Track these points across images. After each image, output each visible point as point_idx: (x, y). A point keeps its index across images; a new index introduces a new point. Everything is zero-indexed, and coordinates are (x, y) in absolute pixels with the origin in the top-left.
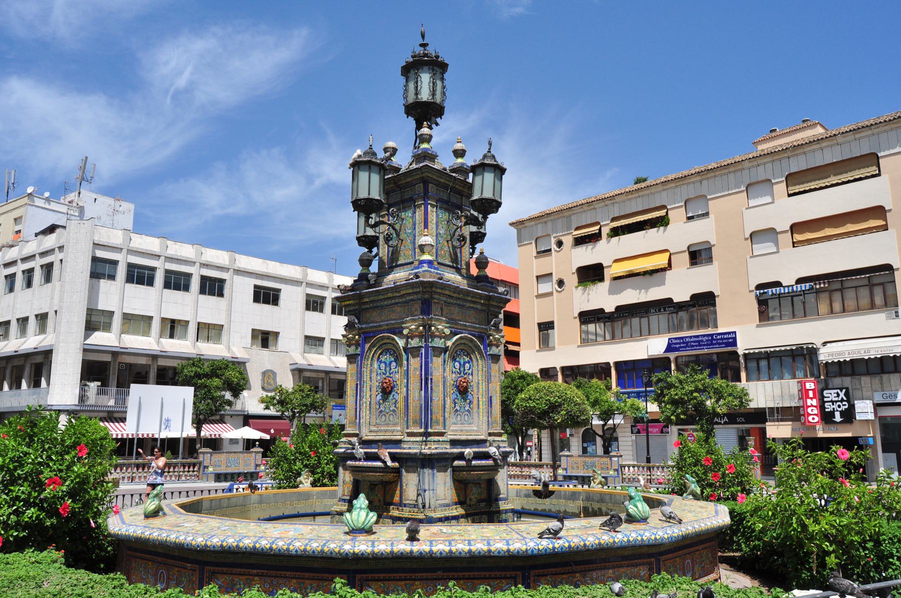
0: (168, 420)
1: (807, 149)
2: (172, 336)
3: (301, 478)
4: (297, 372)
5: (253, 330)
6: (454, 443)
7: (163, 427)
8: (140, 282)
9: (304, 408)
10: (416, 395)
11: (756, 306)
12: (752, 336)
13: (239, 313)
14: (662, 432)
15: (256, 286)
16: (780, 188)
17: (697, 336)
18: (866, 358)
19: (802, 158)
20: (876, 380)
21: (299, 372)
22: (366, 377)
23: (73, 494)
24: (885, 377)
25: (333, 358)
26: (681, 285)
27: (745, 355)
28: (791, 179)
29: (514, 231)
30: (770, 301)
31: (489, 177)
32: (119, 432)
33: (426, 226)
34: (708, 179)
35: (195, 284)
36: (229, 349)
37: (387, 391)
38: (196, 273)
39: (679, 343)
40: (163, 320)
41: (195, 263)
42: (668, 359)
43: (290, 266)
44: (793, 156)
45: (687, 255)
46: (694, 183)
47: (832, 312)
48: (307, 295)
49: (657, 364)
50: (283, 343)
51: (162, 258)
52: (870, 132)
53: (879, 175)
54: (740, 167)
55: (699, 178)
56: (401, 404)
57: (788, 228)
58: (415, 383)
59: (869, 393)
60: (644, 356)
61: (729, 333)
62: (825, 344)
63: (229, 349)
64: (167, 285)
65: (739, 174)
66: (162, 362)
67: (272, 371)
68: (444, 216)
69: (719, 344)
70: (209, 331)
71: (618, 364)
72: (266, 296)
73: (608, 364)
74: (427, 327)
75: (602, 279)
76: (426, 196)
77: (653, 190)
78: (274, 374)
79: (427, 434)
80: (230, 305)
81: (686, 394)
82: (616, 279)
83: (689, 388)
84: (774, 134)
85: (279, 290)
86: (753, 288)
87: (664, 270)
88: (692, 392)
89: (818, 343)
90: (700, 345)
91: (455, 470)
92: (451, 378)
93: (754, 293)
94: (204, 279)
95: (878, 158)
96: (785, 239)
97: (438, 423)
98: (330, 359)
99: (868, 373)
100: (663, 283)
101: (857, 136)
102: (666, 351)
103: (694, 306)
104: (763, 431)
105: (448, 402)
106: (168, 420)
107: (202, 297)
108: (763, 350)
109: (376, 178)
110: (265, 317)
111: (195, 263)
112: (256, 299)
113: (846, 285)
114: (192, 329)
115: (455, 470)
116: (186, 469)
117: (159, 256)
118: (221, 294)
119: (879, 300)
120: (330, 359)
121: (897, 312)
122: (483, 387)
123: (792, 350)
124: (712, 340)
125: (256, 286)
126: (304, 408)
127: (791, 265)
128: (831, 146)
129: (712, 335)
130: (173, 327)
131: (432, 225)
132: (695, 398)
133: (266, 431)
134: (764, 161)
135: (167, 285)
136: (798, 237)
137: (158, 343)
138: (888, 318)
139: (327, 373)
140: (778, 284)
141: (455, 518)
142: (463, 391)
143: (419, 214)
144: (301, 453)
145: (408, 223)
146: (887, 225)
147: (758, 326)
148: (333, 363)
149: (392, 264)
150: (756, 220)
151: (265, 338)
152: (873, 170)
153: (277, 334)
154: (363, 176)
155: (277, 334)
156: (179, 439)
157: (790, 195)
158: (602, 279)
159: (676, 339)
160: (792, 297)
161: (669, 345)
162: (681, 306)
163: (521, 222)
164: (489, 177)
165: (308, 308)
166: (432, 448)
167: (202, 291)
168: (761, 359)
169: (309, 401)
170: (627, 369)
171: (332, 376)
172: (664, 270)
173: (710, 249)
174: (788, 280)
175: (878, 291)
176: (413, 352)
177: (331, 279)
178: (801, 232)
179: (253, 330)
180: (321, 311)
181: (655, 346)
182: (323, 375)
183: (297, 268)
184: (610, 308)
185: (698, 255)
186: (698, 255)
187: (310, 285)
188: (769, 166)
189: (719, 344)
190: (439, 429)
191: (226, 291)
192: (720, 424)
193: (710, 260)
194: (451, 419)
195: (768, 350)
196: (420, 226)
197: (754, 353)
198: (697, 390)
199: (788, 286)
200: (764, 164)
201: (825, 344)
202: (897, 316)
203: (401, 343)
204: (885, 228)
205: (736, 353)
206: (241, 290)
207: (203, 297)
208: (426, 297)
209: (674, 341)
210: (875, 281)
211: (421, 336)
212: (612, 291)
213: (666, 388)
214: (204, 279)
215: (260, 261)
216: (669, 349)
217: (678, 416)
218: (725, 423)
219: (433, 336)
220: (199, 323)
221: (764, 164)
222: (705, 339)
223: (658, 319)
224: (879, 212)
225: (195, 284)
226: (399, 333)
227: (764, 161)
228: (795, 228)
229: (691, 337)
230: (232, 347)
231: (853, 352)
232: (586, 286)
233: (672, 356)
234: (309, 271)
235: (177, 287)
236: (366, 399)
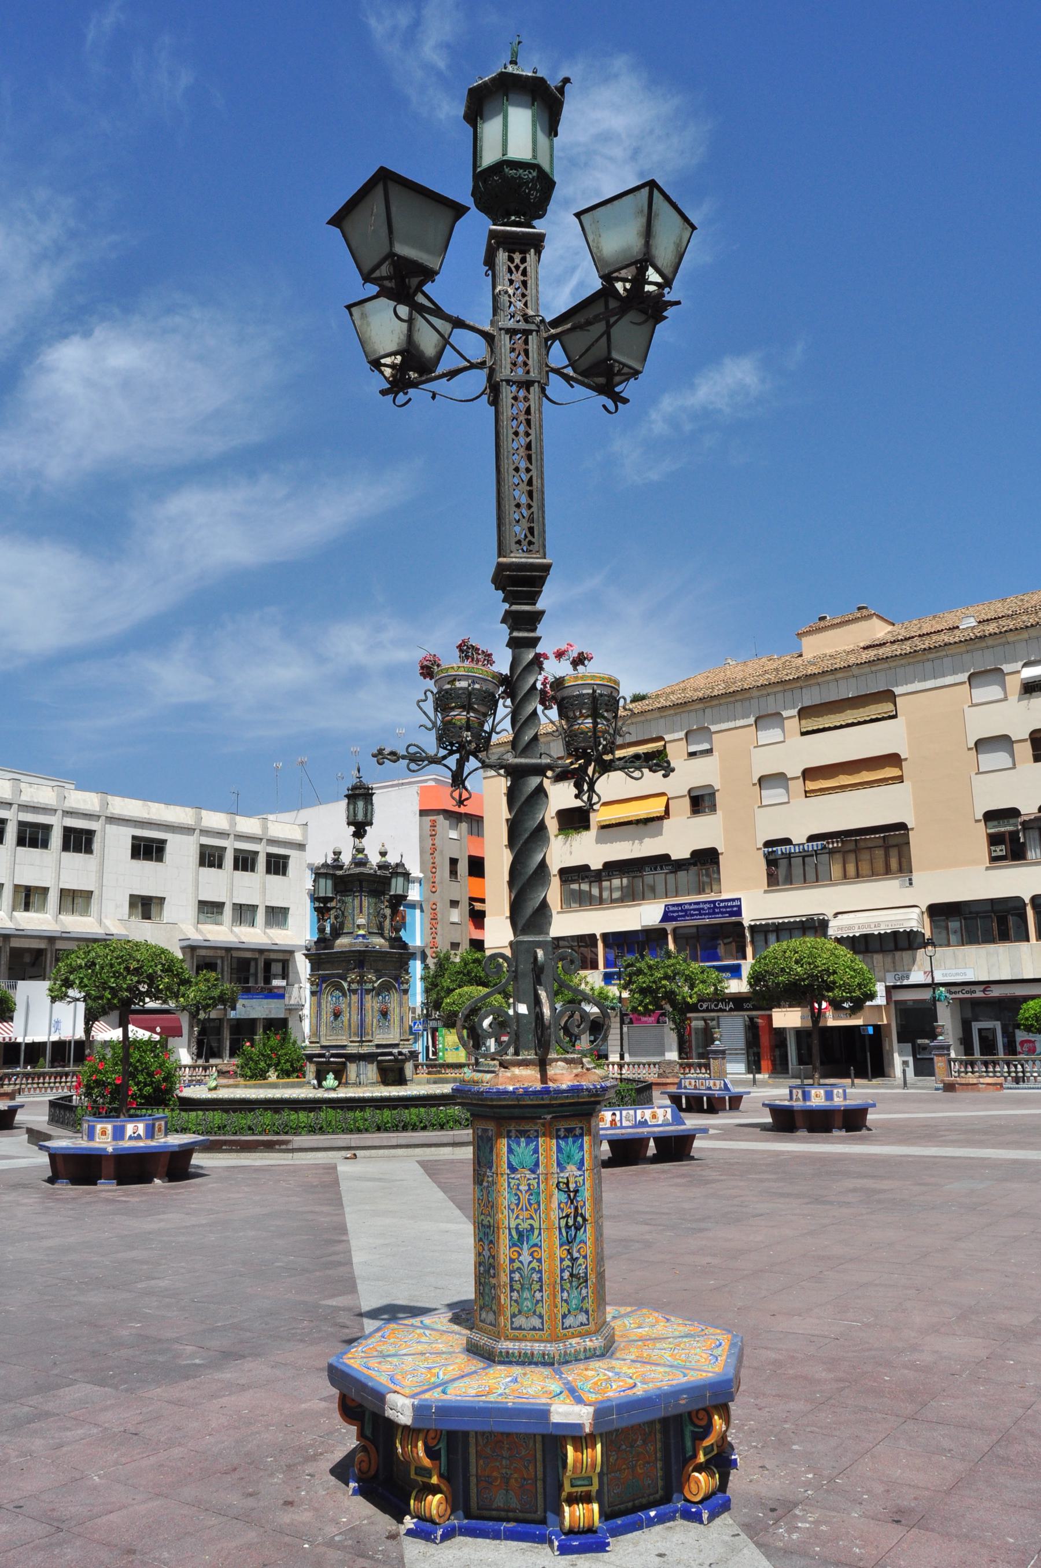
0: (58, 1022)
1: (821, 680)
2: (27, 907)
3: (270, 1073)
5: (131, 896)
6: (378, 1046)
7: (53, 1029)
9: (210, 1002)
10: (355, 1018)
11: (765, 867)
12: (760, 904)
13: (112, 874)
14: (658, 1022)
15: (134, 838)
16: (793, 725)
17: (698, 903)
18: (876, 933)
19: (815, 690)
20: (889, 959)
21: (191, 949)
22: (323, 1006)
23: (165, 1079)
24: (898, 954)
25: (236, 929)
26: (679, 839)
27: (751, 927)
28: (804, 713)
30: (782, 863)
31: (400, 880)
32: (6, 1035)
33: (361, 912)
34: (712, 707)
35: (56, 838)
36: (100, 922)
37: (337, 1015)
38: (57, 824)
39: (677, 911)
40: (17, 887)
41: (56, 810)
42: (664, 930)
43: (178, 808)
44: (806, 686)
45: (687, 800)
46: (696, 711)
47: (845, 877)
48: (202, 846)
49: (646, 940)
50: (169, 912)
51: (15, 807)
52: (886, 665)
53: (895, 717)
54: (747, 695)
55: (701, 706)
56: (346, 1023)
57: (799, 774)
58: (354, 1012)
59: (881, 974)
60: (637, 927)
61: (733, 900)
62: (836, 915)
63: (100, 922)
65: (746, 704)
66: (15, 943)
68: (373, 900)
69: (722, 913)
70: (75, 899)
71: (605, 936)
72: (147, 850)
73: (594, 935)
74: (362, 976)
75: (587, 827)
76: (361, 891)
77: (649, 716)
79: (362, 1041)
80: (102, 864)
81: (654, 982)
82: (604, 827)
83: (658, 975)
84: (822, 624)
85: (164, 842)
86: (760, 845)
87: (660, 818)
88: (661, 979)
89: (829, 915)
90: (700, 914)
91: (379, 1062)
92: (376, 1006)
93: (761, 852)
94: (68, 831)
95: (895, 696)
96: (797, 786)
98: (232, 931)
99: (882, 950)
100: (659, 833)
101: (874, 668)
102: (662, 921)
103: (695, 865)
104: (770, 1018)
105: (375, 1020)
106: (58, 1022)
107: (65, 854)
108: (770, 921)
109: (330, 883)
110: (146, 879)
111: (56, 810)
113: (862, 844)
114: (53, 897)
115: (379, 1062)
116: (52, 1080)
117: (11, 804)
118: (89, 850)
119: (894, 864)
120: (232, 931)
121: (910, 880)
122: (397, 1010)
123: (802, 921)
124: (714, 908)
125: (134, 838)
126: (210, 1002)
127: (804, 819)
128: (847, 678)
129: (714, 902)
130: (244, 913)
131: (365, 909)
132: (664, 986)
133: (152, 1030)
134: (775, 690)
136: (811, 785)
137: (11, 918)
138: (902, 886)
139: (228, 950)
140: (787, 841)
141: (475, 1372)
142: (384, 1014)
143: (357, 902)
144: (263, 1055)
145: (350, 906)
146: (902, 776)
147: (766, 892)
148: (236, 936)
149: (337, 932)
150: (764, 763)
151: (145, 906)
152: (887, 707)
153: (162, 900)
154: (322, 881)
155: (162, 900)
156: (44, 1044)
157: (803, 734)
158: (587, 827)
159: (673, 905)
160: (804, 857)
161: (666, 913)
162: (679, 865)
164: (400, 880)
165: (202, 863)
166: (364, 1050)
167: (66, 847)
168: (768, 931)
169: (216, 993)
170: (617, 941)
171: (235, 954)
172: (660, 818)
173: (714, 794)
174: (799, 837)
175: (894, 853)
176: (355, 992)
177: (233, 824)
178: (813, 779)
179: (131, 896)
180: (220, 866)
181: (646, 915)
182: (223, 953)
183: (188, 809)
184: (596, 865)
185: (701, 802)
186: (701, 802)
187: (205, 832)
188: (780, 696)
189: (722, 913)
190: (369, 1038)
191: (96, 846)
192: (725, 1010)
193: (713, 808)
194: (376, 1031)
195: (776, 921)
196: (357, 911)
197: (761, 925)
198: (666, 977)
199: (799, 845)
200: (775, 693)
201: (836, 915)
202: (911, 884)
203: (345, 985)
204: (900, 779)
205: (740, 924)
206: (115, 843)
208: (361, 959)
209: (671, 909)
210: (892, 842)
211: (358, 982)
212: (599, 840)
213: (635, 974)
214: (68, 831)
215: (139, 803)
216: (666, 917)
217: (646, 1007)
218: (731, 1010)
219: (366, 982)
220: (62, 890)
221: (775, 693)
222: (706, 906)
223: (657, 878)
224: (893, 760)
225: (56, 838)
226: (345, 980)
227: (775, 690)
228: (808, 774)
229: (690, 904)
230: (104, 920)
231: (863, 925)
232: (567, 836)
233: (669, 926)
234: (204, 813)
235: (34, 844)
236: (324, 1019)
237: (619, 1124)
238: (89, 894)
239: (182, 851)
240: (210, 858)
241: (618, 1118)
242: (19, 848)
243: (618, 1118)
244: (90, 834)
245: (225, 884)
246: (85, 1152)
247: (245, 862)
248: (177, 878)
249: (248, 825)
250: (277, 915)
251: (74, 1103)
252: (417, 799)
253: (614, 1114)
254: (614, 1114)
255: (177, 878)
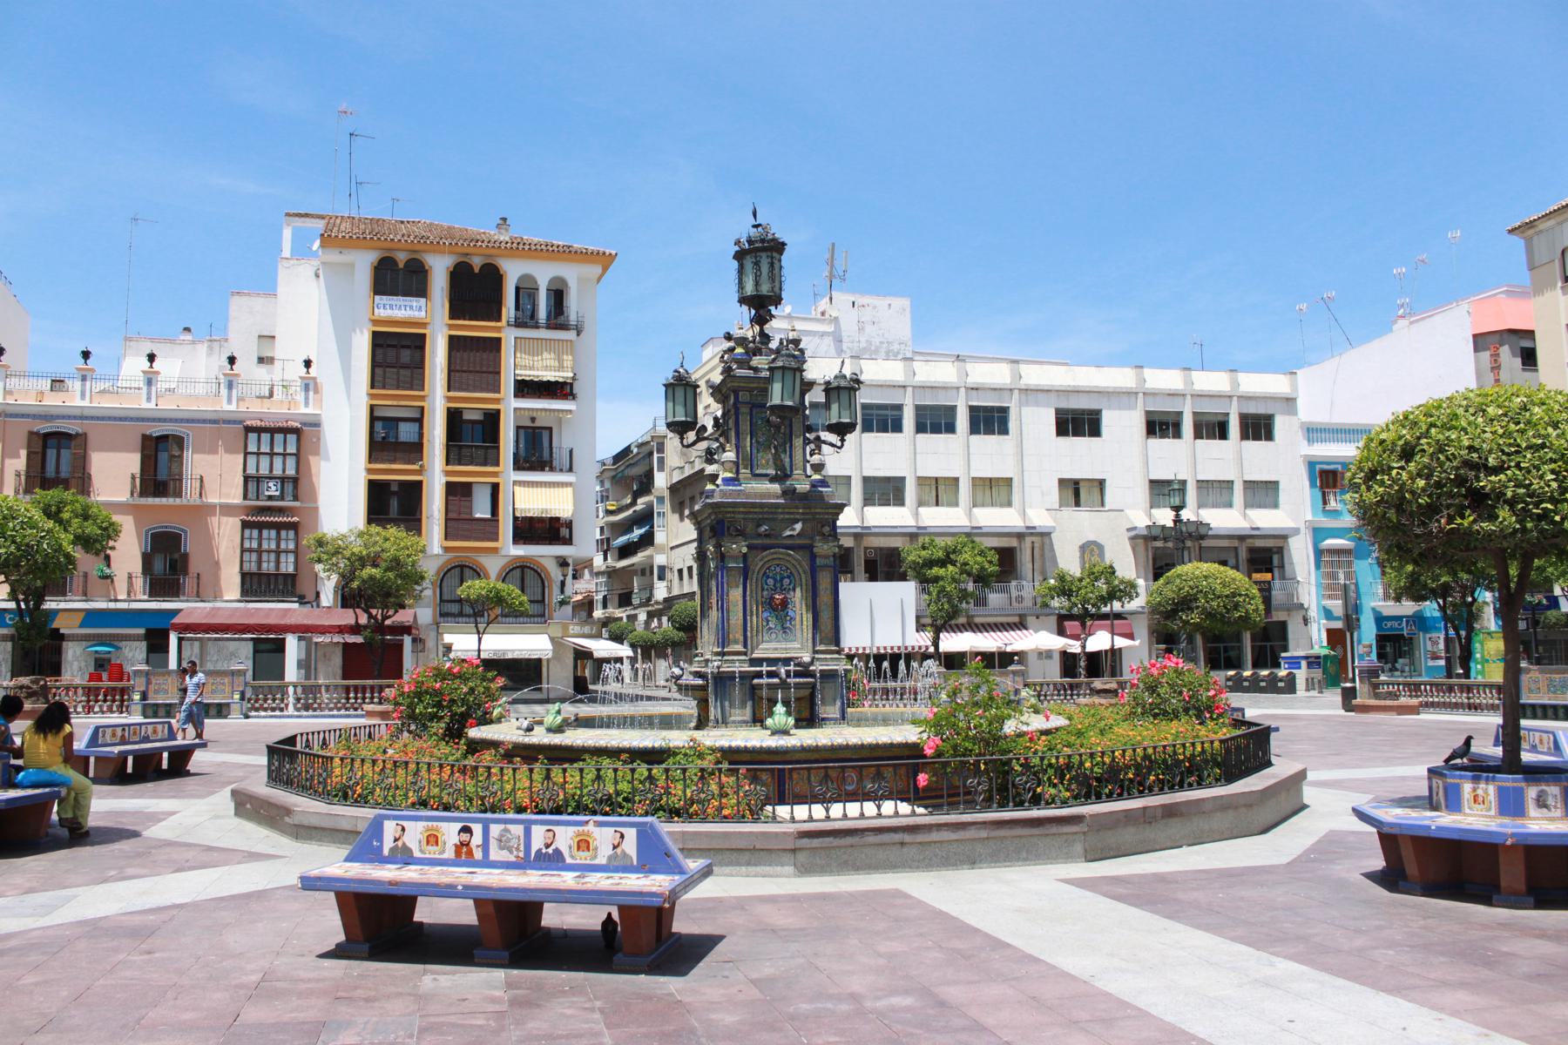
4: (1141, 541)
8: (936, 429)
13: (1036, 454)
29: (1518, 242)
35: (962, 421)
64: (974, 429)
67: (1095, 543)
70: (995, 489)
72: (1078, 422)
78: (1100, 547)
97: (736, 642)
107: (974, 438)
110: (1079, 456)
112: (1062, 430)
118: (1004, 430)
120: (1245, 515)
130: (939, 489)
135: (974, 429)
137: (970, 515)
151: (1075, 491)
163: (1530, 225)
177: (1235, 384)
191: (1012, 425)
206: (1123, 425)
207: (977, 439)
225: (962, 421)
237: (478, 855)
238: (1009, 481)
239: (1123, 425)
240: (1161, 426)
241: (477, 839)
242: (920, 436)
243: (477, 839)
244: (1004, 411)
245: (1178, 458)
246: (1455, 836)
247: (1213, 428)
248: (1122, 456)
249: (1212, 381)
250: (1263, 492)
251: (298, 748)
252: (1468, 320)
253: (466, 830)
254: (466, 830)
255: (1122, 456)
